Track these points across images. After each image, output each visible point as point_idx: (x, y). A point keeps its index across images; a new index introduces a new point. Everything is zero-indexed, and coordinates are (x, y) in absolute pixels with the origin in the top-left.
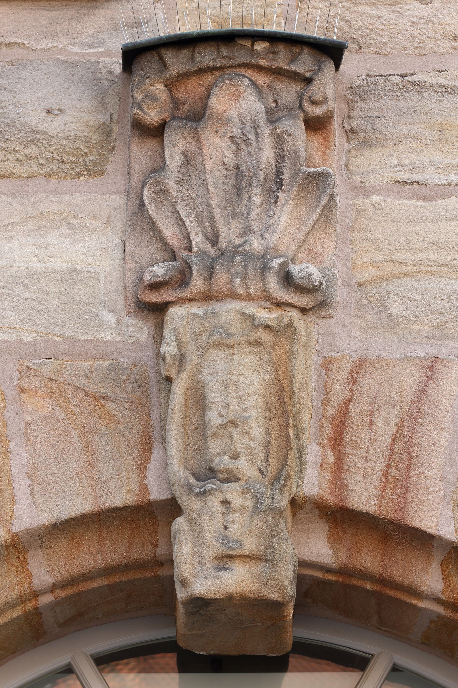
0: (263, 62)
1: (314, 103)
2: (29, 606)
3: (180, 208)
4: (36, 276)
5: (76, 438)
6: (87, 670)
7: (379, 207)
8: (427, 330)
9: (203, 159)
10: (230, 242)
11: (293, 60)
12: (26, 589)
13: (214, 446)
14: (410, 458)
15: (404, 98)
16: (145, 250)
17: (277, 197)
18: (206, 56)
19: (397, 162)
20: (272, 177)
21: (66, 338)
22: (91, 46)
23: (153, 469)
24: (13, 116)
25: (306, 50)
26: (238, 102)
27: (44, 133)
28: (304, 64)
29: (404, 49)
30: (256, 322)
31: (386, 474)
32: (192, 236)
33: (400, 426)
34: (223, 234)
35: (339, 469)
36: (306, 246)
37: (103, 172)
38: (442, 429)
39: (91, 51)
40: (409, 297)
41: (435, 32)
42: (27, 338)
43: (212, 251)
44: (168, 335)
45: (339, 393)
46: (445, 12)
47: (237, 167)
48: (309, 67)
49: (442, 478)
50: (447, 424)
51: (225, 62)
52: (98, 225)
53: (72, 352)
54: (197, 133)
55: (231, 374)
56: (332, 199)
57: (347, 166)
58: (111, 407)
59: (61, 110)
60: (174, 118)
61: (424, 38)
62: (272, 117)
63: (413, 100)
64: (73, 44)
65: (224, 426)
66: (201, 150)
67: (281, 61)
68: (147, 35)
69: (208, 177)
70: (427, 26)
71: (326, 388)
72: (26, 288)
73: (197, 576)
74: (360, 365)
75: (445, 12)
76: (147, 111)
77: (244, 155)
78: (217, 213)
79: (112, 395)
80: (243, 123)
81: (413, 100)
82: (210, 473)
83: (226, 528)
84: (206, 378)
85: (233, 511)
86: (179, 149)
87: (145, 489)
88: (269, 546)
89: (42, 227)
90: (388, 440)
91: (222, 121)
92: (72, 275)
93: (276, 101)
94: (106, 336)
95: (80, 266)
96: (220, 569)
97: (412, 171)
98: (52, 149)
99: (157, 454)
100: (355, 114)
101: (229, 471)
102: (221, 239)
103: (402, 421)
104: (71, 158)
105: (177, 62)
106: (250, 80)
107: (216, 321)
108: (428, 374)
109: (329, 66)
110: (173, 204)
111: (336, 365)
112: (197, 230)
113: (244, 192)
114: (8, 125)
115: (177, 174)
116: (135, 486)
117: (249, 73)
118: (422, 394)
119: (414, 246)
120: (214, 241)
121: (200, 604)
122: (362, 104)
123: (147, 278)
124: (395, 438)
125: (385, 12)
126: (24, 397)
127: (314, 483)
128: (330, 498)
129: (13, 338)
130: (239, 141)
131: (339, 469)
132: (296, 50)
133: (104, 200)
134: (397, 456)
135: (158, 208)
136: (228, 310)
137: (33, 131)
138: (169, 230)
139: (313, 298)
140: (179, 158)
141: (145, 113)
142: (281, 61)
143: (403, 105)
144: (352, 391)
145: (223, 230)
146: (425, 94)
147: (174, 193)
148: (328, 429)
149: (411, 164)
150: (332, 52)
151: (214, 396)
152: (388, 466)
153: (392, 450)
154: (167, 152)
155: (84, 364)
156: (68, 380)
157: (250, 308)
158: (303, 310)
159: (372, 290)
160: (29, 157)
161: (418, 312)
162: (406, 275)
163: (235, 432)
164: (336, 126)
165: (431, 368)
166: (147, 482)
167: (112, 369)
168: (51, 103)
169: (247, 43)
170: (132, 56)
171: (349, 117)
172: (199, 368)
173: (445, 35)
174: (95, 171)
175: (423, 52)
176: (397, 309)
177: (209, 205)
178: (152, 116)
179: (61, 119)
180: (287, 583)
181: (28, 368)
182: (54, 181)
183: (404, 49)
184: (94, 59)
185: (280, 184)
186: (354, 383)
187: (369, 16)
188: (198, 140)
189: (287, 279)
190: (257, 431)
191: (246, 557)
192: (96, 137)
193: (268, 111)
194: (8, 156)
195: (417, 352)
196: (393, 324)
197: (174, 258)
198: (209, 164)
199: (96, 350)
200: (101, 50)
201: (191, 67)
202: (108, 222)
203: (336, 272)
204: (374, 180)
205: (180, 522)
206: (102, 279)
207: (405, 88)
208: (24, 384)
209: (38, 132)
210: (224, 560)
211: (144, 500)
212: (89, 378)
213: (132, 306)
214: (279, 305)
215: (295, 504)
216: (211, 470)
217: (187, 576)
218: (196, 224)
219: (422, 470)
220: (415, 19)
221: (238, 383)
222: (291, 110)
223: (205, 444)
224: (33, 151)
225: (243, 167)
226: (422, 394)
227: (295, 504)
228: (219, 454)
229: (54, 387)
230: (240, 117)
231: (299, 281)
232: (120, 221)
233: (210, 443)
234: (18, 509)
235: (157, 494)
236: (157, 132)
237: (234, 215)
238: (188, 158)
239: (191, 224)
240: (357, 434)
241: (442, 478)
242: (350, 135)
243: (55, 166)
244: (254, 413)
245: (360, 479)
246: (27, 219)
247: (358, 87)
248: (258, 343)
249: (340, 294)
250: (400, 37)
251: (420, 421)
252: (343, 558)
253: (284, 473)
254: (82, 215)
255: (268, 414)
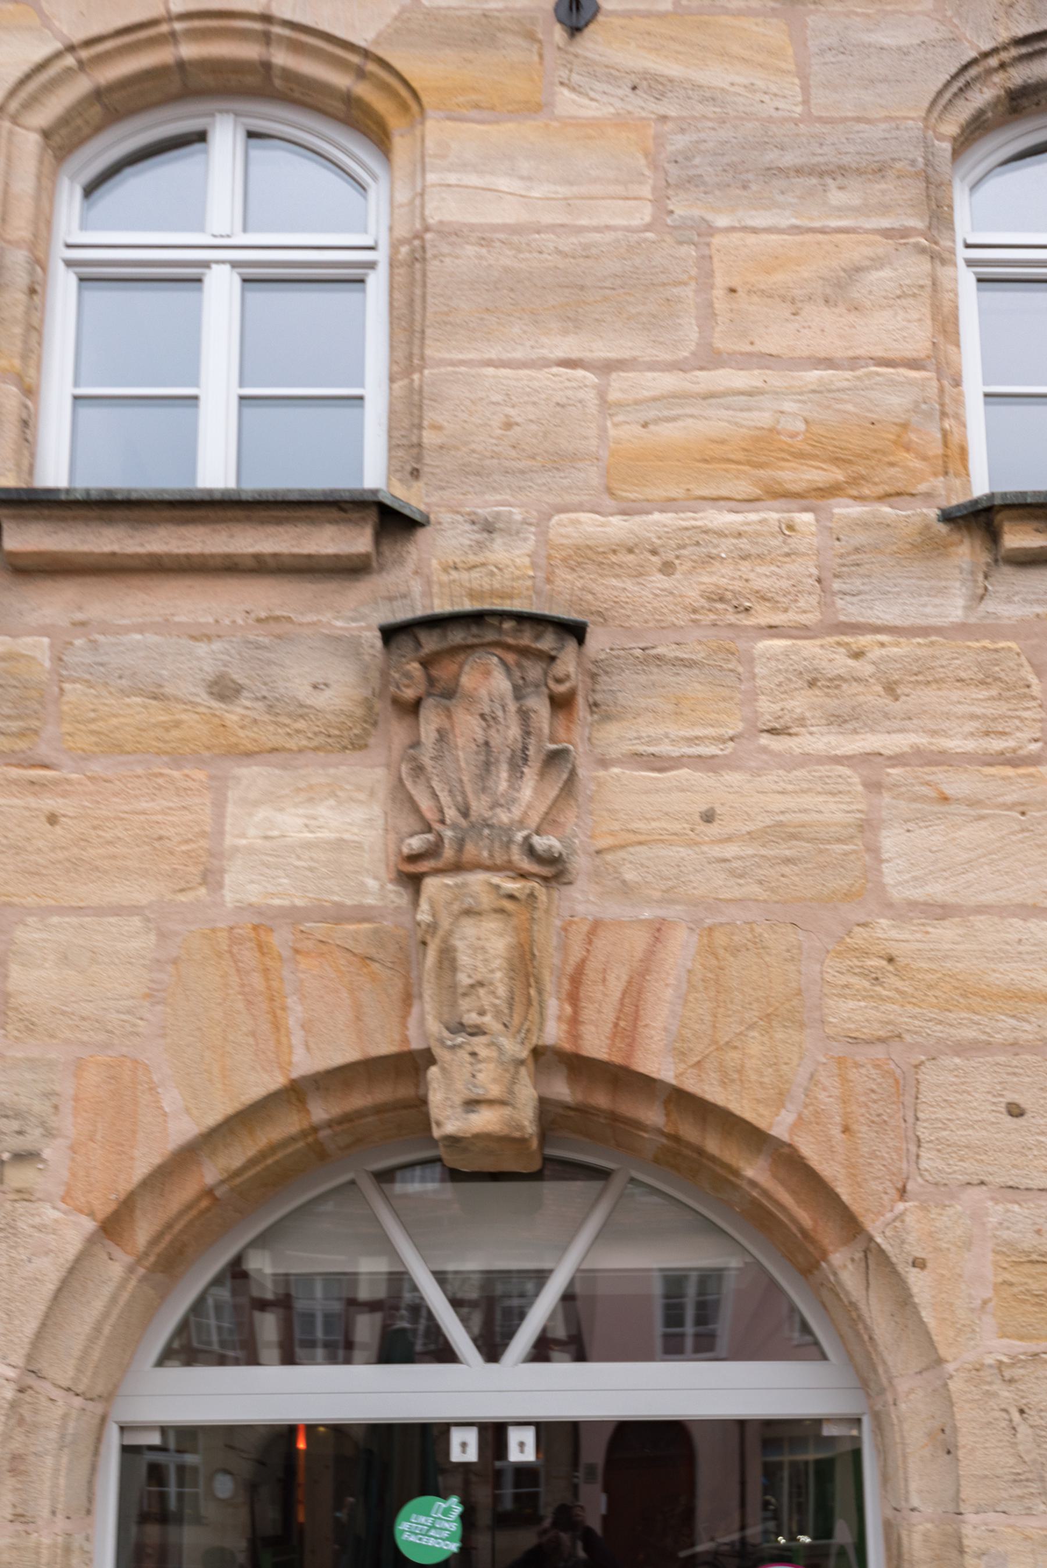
0: (511, 641)
1: (559, 681)
2: (310, 1139)
3: (434, 784)
4: (308, 845)
5: (345, 994)
6: (368, 1186)
7: (618, 778)
8: (657, 895)
9: (455, 736)
10: (480, 815)
11: (538, 637)
12: (305, 1125)
13: (464, 1004)
14: (637, 1012)
15: (644, 670)
16: (406, 822)
17: (522, 772)
18: (457, 636)
19: (635, 735)
20: (519, 753)
21: (336, 904)
22: (354, 620)
23: (412, 1022)
24: (282, 691)
25: (550, 629)
26: (488, 680)
27: (310, 707)
28: (547, 643)
29: (646, 622)
30: (502, 892)
31: (616, 1025)
32: (446, 810)
33: (629, 983)
34: (474, 808)
35: (574, 1021)
36: (550, 817)
37: (366, 746)
38: (667, 985)
39: (354, 625)
40: (642, 865)
41: (676, 605)
42: (299, 902)
43: (463, 823)
44: (424, 905)
45: (577, 952)
46: (686, 583)
47: (487, 744)
48: (554, 645)
49: (665, 1029)
50: (672, 981)
51: (476, 641)
52: (362, 796)
53: (340, 915)
54: (448, 710)
55: (479, 939)
56: (573, 773)
57: (589, 739)
58: (375, 966)
59: (326, 685)
60: (429, 694)
61: (665, 611)
62: (518, 694)
63: (651, 673)
64: (336, 618)
65: (472, 986)
66: (453, 727)
67: (526, 639)
68: (402, 614)
69: (460, 753)
70: (668, 599)
71: (564, 948)
72: (299, 858)
73: (448, 1118)
74: (596, 926)
75: (686, 583)
76: (403, 689)
77: (493, 732)
78: (469, 788)
79: (376, 956)
80: (492, 701)
81: (651, 673)
82: (460, 1028)
83: (474, 1076)
84: (459, 944)
85: (480, 1061)
86: (433, 727)
87: (405, 1040)
88: (511, 1092)
89: (311, 800)
90: (618, 995)
91: (471, 699)
92: (339, 845)
93: (523, 678)
94: (370, 901)
95: (346, 836)
96: (468, 1112)
97: (648, 743)
98: (319, 723)
99: (415, 1010)
100: (598, 687)
101: (477, 1026)
102: (472, 813)
103: (632, 978)
104: (337, 732)
105: (430, 642)
106: (500, 658)
107: (465, 891)
108: (657, 935)
109: (571, 645)
110: (428, 780)
111: (574, 927)
112: (451, 804)
113: (493, 768)
114: (277, 699)
115: (431, 750)
116: (397, 1037)
117: (498, 651)
118: (650, 954)
119: (648, 816)
120: (465, 813)
121: (453, 1141)
122: (605, 678)
123: (406, 851)
124: (624, 993)
125: (629, 584)
126: (298, 957)
127: (553, 1033)
128: (567, 1046)
129: (286, 903)
130: (488, 718)
131: (574, 1021)
132: (541, 628)
133: (371, 773)
134: (626, 1010)
135: (415, 782)
136: (477, 880)
137: (301, 706)
138: (425, 804)
139: (553, 869)
140: (434, 735)
141: (401, 691)
142: (526, 639)
143: (642, 679)
144: (588, 951)
145: (474, 805)
146: (664, 668)
147: (430, 769)
148: (566, 984)
149: (649, 736)
150: (576, 631)
151: (464, 959)
152: (618, 1018)
153: (622, 1004)
154: (422, 730)
155: (352, 927)
156: (338, 943)
157: (496, 879)
158: (545, 879)
159: (609, 857)
160: (298, 731)
161: (650, 878)
162: (640, 843)
163: (482, 991)
164: (580, 701)
165: (659, 930)
166: (408, 1033)
167: (376, 931)
168: (318, 677)
169: (494, 621)
170: (390, 634)
171: (594, 691)
172: (450, 933)
173: (685, 608)
174: (358, 745)
175: (663, 625)
176: (630, 876)
177: (461, 781)
178: (409, 694)
179: (328, 693)
180: (526, 1123)
181: (302, 931)
182: (322, 754)
183: (646, 622)
184: (356, 633)
185: (525, 759)
186: (590, 942)
187: (614, 588)
188: (449, 717)
189: (531, 851)
190: (502, 991)
191: (491, 1102)
192: (360, 712)
193: (516, 688)
194: (280, 730)
195: (646, 914)
196: (626, 890)
197: (429, 829)
198: (460, 742)
199: (362, 914)
200: (363, 624)
201: (445, 645)
202: (372, 793)
203: (577, 841)
204: (614, 753)
205: (433, 1071)
206: (366, 847)
207: (645, 661)
208: (298, 946)
209: (306, 706)
210: (472, 1104)
211: (405, 1049)
212: (356, 940)
213: (393, 875)
214: (523, 876)
215: (537, 1052)
216: (462, 1024)
217: (441, 1118)
218: (449, 799)
219: (648, 1021)
220: (658, 592)
221: (484, 948)
222: (537, 686)
223: (456, 1002)
224: (301, 725)
225: (492, 743)
226: (650, 954)
227: (537, 1052)
228: (469, 1011)
229: (324, 948)
230: (490, 694)
231: (541, 853)
232: (382, 792)
233: (461, 1002)
234: (295, 1059)
235: (416, 1044)
236: (412, 709)
237: (484, 790)
238: (442, 736)
239: (444, 798)
240: (591, 989)
241: (665, 1029)
242: (594, 709)
243: (321, 740)
244: (499, 975)
245: (593, 1029)
246: (299, 790)
247: (602, 661)
248: (502, 911)
249: (580, 864)
250: (643, 610)
251: (648, 978)
252: (580, 1097)
253: (525, 1027)
254: (348, 787)
255: (512, 974)
